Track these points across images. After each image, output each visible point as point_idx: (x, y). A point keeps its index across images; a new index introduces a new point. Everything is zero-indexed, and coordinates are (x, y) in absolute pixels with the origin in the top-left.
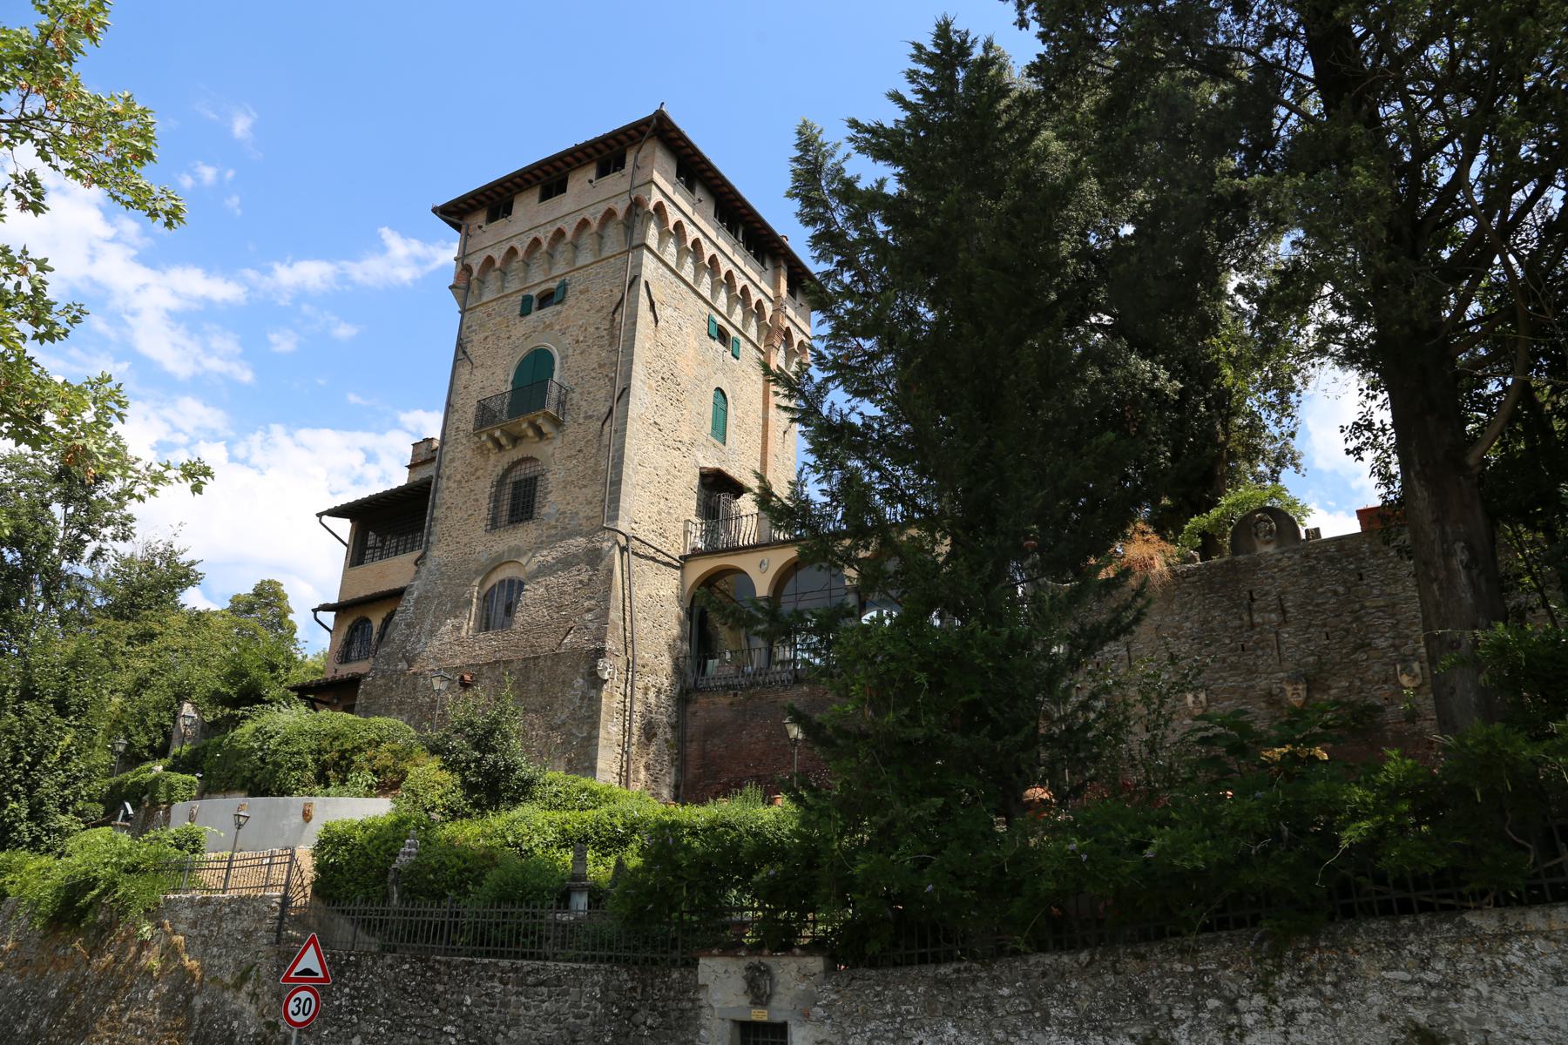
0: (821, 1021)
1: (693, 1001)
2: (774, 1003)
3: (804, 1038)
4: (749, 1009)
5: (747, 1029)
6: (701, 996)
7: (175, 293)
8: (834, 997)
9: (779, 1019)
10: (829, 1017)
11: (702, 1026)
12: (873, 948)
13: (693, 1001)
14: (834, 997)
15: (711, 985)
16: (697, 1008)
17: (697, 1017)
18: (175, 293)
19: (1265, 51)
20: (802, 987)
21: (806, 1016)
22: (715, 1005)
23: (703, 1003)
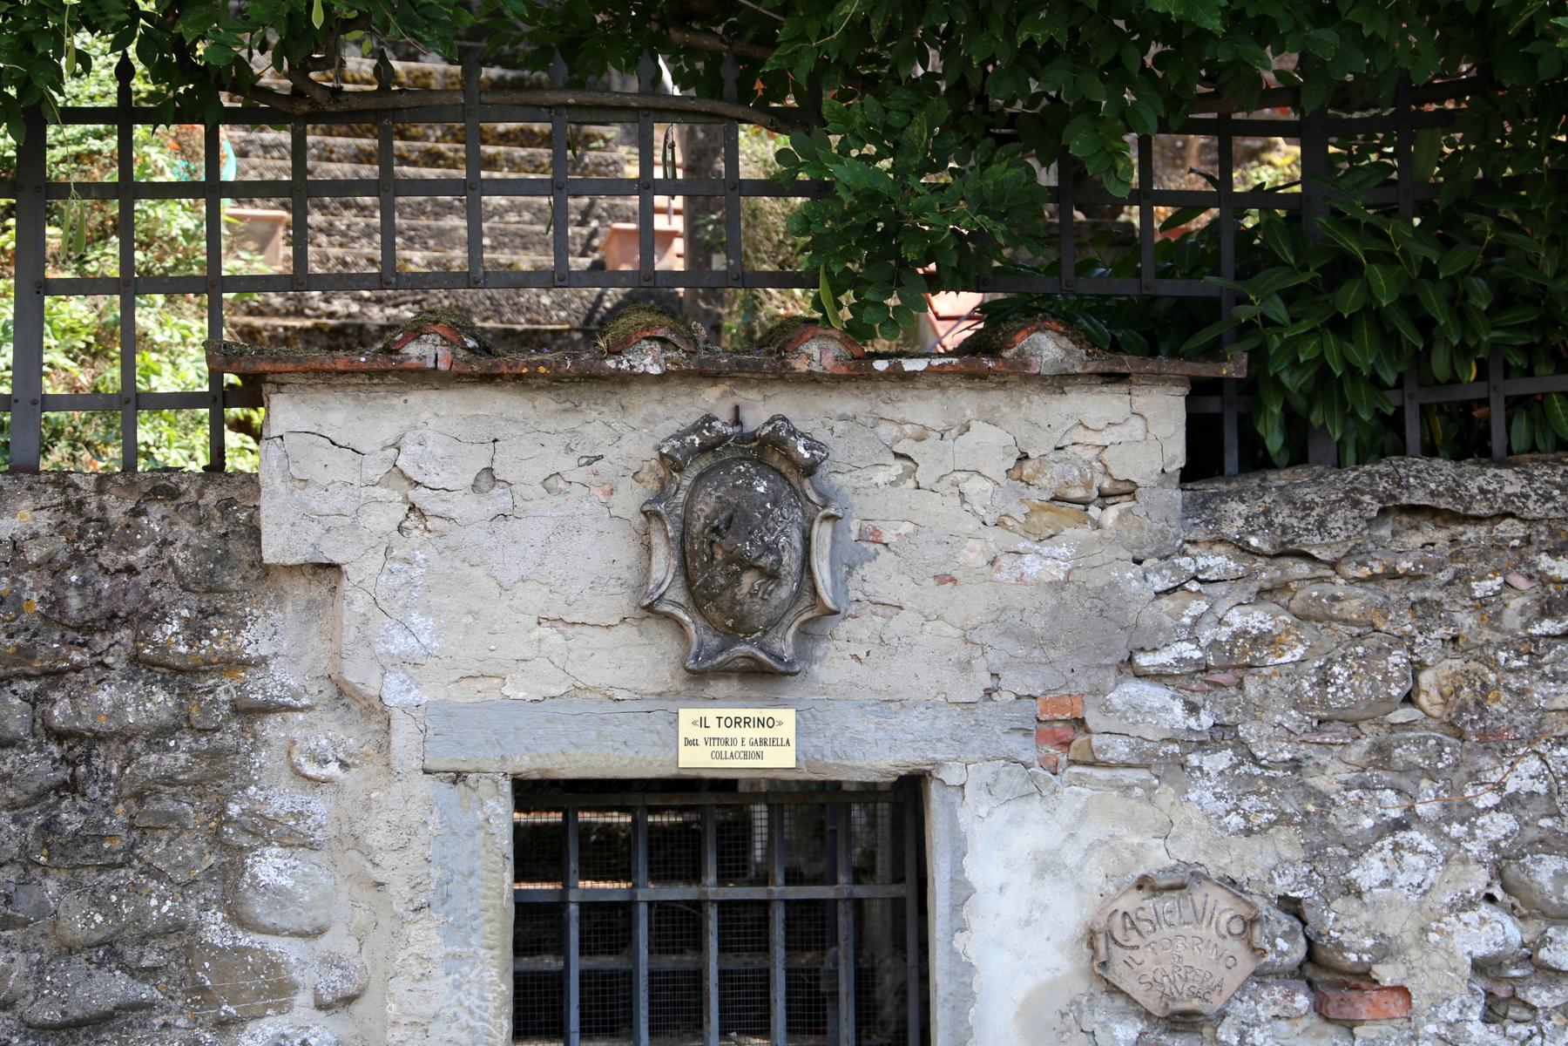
0: (1168, 762)
1: (180, 676)
2: (835, 665)
3: (1046, 866)
4: (669, 699)
5: (591, 847)
6: (253, 641)
7: (1270, 163)
8: (1258, 619)
9: (873, 757)
10: (1223, 735)
11: (263, 830)
12: (241, 478)
13: (180, 676)
14: (1258, 619)
15: (363, 568)
16: (221, 714)
17: (219, 772)
18: (1270, 163)
19: (1537, 340)
20: (1044, 564)
21: (1064, 735)
22: (395, 691)
23: (280, 680)
